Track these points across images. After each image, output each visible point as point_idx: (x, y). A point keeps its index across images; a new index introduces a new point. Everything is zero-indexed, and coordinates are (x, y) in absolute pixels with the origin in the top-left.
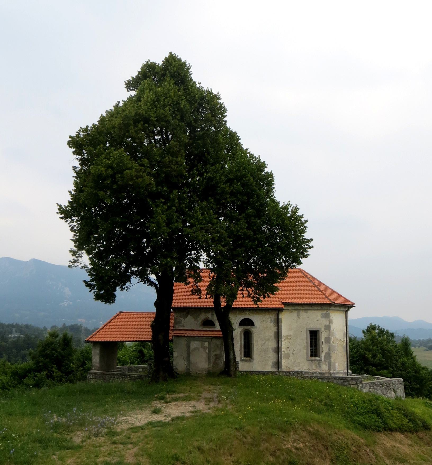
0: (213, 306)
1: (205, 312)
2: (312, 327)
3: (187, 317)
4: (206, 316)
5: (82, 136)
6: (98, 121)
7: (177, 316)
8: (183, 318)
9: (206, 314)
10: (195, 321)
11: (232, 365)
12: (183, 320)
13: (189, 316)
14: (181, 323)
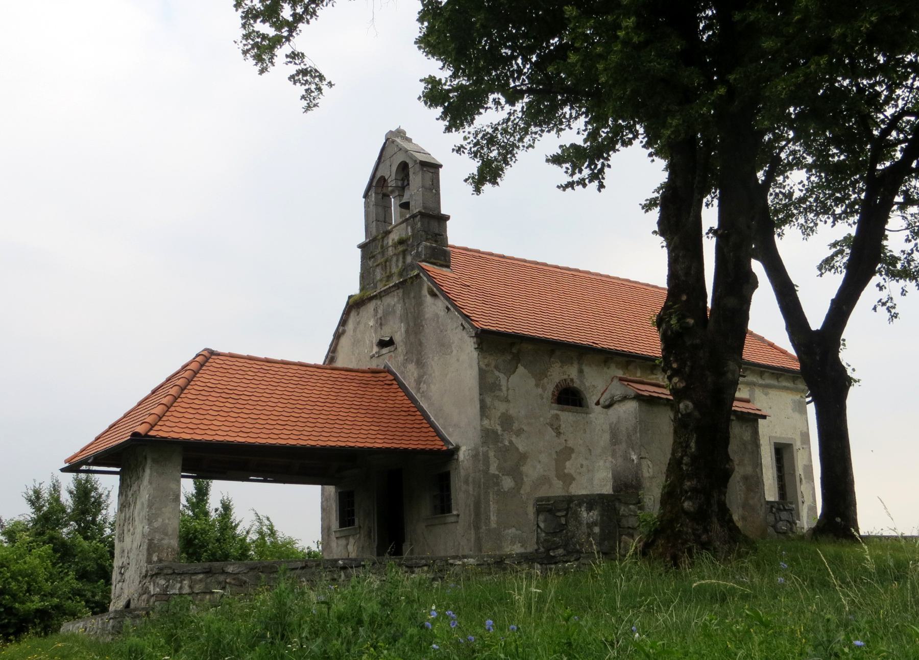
0: (799, 368)
1: (562, 362)
2: (778, 435)
3: (514, 372)
4: (564, 373)
5: (887, 93)
6: (291, 15)
7: (486, 365)
8: (505, 374)
9: (565, 367)
10: (537, 386)
11: (145, 544)
12: (502, 377)
13: (521, 369)
14: (500, 390)
